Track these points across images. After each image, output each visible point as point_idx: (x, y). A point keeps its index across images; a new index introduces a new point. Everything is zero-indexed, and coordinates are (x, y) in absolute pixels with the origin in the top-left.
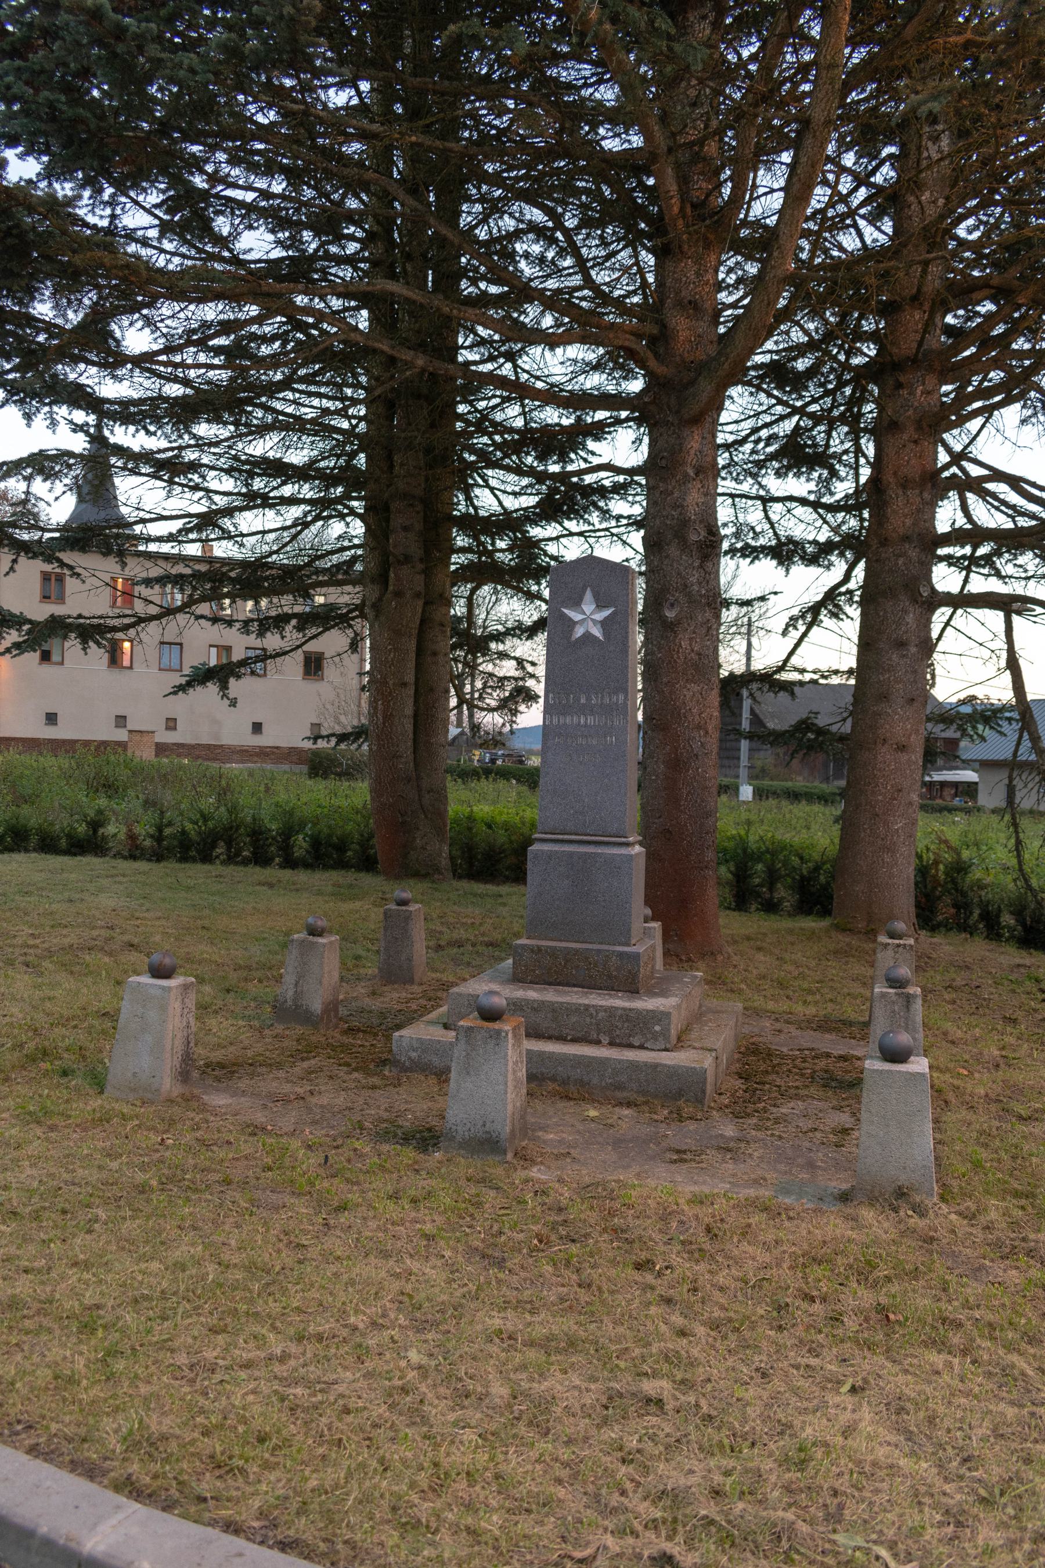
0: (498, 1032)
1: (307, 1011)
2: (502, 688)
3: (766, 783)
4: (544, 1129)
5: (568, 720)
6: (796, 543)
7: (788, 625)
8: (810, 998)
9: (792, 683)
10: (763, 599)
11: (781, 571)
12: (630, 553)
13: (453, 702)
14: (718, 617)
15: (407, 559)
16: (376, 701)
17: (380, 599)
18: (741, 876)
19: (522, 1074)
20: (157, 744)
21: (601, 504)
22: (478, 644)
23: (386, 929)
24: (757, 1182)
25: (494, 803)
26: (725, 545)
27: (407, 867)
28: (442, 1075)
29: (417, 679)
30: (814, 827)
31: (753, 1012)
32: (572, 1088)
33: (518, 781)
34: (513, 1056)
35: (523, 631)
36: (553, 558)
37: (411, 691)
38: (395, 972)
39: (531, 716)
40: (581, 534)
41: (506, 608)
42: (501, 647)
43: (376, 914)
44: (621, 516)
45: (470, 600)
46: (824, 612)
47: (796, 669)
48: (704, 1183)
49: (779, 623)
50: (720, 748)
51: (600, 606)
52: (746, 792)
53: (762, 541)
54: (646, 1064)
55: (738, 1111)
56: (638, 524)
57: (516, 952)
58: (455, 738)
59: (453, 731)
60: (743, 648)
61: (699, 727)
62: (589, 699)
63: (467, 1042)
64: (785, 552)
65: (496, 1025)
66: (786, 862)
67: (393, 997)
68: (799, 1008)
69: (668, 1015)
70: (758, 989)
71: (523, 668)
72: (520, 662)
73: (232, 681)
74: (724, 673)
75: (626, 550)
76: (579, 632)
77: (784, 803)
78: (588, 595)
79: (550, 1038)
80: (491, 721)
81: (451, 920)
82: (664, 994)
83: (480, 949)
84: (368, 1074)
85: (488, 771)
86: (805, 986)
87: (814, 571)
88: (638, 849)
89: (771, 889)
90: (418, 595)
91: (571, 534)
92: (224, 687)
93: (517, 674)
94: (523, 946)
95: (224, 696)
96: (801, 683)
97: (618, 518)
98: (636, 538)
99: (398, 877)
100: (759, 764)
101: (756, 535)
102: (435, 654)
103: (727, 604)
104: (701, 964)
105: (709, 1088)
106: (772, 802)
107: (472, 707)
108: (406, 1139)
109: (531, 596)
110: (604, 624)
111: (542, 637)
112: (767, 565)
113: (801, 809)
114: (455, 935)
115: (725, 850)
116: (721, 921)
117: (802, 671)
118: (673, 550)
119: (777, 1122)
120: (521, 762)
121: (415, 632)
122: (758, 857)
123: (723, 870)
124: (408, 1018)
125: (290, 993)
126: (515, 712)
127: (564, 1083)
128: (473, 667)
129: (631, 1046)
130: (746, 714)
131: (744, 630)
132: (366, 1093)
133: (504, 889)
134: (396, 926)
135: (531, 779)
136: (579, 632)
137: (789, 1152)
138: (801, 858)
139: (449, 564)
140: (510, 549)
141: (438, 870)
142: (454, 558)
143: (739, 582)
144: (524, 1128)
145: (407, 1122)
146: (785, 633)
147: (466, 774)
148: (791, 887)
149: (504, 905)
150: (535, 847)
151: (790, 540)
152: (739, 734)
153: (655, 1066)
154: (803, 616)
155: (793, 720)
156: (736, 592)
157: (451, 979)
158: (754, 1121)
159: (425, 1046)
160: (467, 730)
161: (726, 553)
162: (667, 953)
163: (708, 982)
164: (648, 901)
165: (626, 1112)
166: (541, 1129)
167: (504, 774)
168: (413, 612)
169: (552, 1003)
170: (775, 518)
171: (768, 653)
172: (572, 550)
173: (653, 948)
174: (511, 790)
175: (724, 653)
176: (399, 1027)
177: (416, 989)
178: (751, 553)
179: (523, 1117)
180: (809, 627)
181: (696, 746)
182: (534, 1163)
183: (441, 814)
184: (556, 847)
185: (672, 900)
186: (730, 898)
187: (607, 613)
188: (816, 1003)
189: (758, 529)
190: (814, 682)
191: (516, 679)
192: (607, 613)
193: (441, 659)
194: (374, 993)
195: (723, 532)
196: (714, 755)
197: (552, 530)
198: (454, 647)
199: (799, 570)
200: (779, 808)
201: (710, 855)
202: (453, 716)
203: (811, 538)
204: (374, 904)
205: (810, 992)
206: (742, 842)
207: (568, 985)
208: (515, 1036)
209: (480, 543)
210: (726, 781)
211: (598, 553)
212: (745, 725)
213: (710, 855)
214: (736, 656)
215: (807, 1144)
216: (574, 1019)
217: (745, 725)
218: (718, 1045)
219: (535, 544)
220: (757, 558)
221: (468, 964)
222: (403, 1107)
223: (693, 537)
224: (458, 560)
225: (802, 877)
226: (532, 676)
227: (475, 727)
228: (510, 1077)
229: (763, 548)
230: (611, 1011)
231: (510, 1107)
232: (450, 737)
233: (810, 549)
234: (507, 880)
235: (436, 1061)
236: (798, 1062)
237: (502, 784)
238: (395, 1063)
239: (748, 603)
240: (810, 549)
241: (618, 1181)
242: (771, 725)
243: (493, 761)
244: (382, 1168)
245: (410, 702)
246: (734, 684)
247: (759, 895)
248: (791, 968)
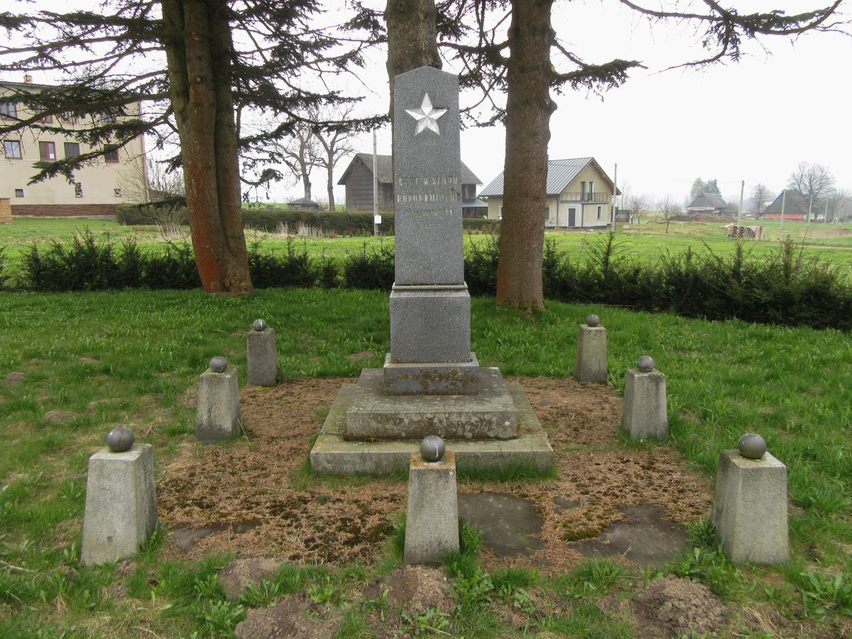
1: (221, 429)
20: (12, 206)
29: (217, 165)
37: (213, 172)
62: (430, 181)
73: (74, 172)
76: (420, 129)
78: (426, 100)
92: (69, 175)
95: (71, 182)
102: (227, 146)
110: (439, 121)
125: (205, 418)
136: (420, 129)
184: (411, 295)
187: (441, 113)
192: (441, 113)
245: (214, 179)
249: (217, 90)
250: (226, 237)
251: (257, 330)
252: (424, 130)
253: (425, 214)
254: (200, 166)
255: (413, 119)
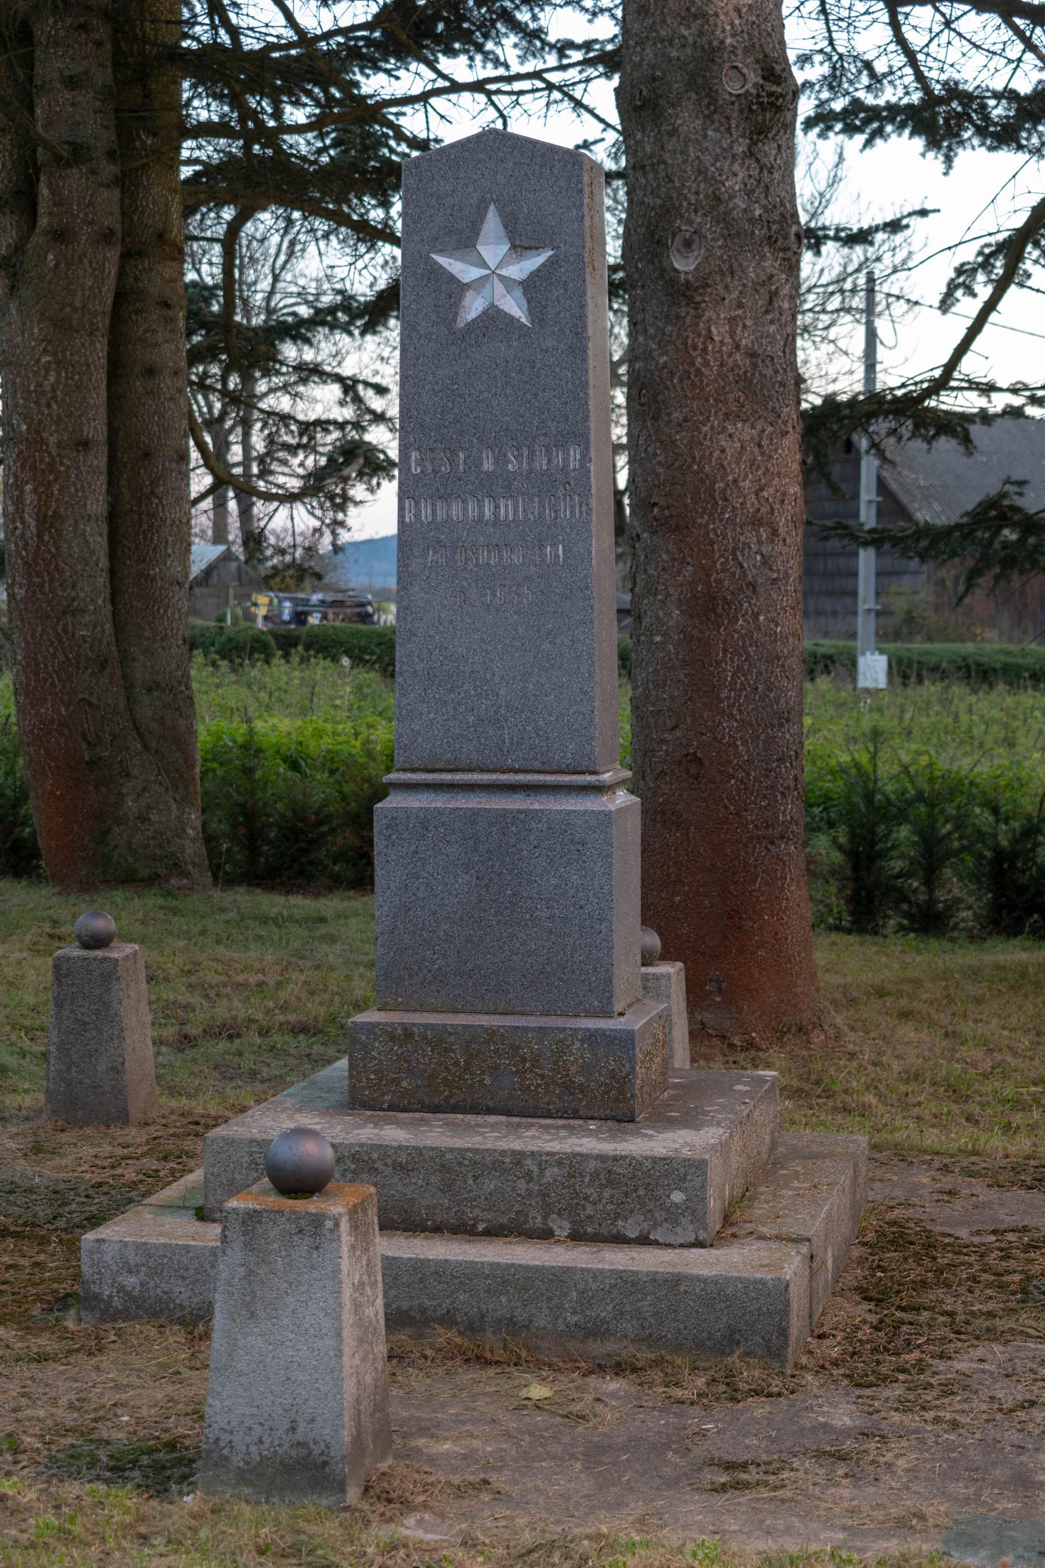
0: (317, 1221)
2: (310, 447)
3: (918, 646)
4: (428, 1430)
5: (456, 510)
6: (967, 98)
7: (952, 287)
8: (1018, 1119)
9: (965, 418)
10: (895, 226)
11: (934, 161)
12: (591, 129)
13: (201, 481)
14: (794, 268)
15: (78, 154)
16: (18, 485)
17: (19, 248)
18: (863, 857)
19: (376, 1309)
21: (523, 16)
22: (253, 348)
23: (59, 1003)
24: (902, 1525)
25: (304, 711)
26: (806, 106)
27: (106, 862)
28: (195, 1323)
30: (1024, 741)
31: (891, 1155)
32: (490, 1337)
33: (358, 660)
34: (352, 1271)
35: (354, 315)
36: (415, 143)
37: (99, 459)
38: (85, 1100)
39: (375, 513)
40: (478, 87)
41: (318, 263)
42: (309, 355)
43: (38, 972)
44: (570, 45)
45: (230, 241)
46: (1031, 252)
47: (973, 385)
48: (788, 1531)
49: (930, 280)
50: (808, 572)
51: (519, 247)
52: (873, 669)
53: (889, 95)
54: (654, 1278)
55: (862, 1368)
56: (608, 60)
57: (354, 1043)
58: (209, 571)
59: (203, 553)
60: (857, 344)
61: (756, 522)
62: (500, 460)
63: (248, 1246)
64: (942, 118)
65: (312, 1205)
66: (960, 823)
67: (81, 1156)
68: (995, 1142)
69: (700, 1166)
70: (904, 1103)
71: (358, 400)
72: (349, 386)
74: (812, 400)
75: (582, 121)
76: (473, 307)
77: (958, 690)
78: (492, 222)
79: (437, 1229)
80: (289, 523)
81: (213, 978)
82: (691, 1120)
83: (278, 1039)
84: (29, 1329)
85: (288, 641)
86: (1009, 1091)
87: (1008, 159)
88: (622, 798)
89: (929, 882)
90: (107, 236)
91: (456, 87)
93: (348, 413)
94: (371, 1027)
96: (984, 417)
97: (563, 47)
98: (602, 93)
99: (87, 887)
100: (900, 605)
101: (877, 80)
102: (151, 372)
103: (815, 239)
104: (776, 1054)
105: (796, 1325)
106: (931, 689)
107: (246, 493)
108: (118, 1469)
109: (370, 235)
110: (530, 286)
111: (393, 330)
112: (903, 147)
113: (992, 704)
114: (222, 1012)
115: (827, 799)
116: (820, 957)
117: (988, 389)
118: (687, 119)
119: (947, 1390)
120: (365, 618)
121: (103, 322)
122: (895, 812)
123: (822, 843)
124: (112, 1200)
126: (342, 503)
127: (473, 1327)
128: (242, 401)
129: (619, 1240)
130: (868, 492)
131: (858, 302)
132: (24, 1370)
133: (331, 904)
134: (83, 993)
135: (374, 652)
136: (473, 307)
137: (976, 1456)
138: (995, 810)
139: (176, 163)
140: (315, 125)
141: (177, 868)
142: (188, 149)
143: (843, 195)
144: (382, 1433)
145: (120, 1431)
146: (946, 304)
147: (240, 650)
148: (975, 877)
149: (332, 939)
150: (393, 802)
151: (953, 91)
152: (857, 538)
153: (674, 1282)
154: (986, 265)
155: (970, 501)
156: (841, 213)
157: (213, 1108)
158: (897, 1391)
159: (156, 1261)
160: (238, 549)
161: (809, 124)
162: (698, 1034)
163: (796, 1094)
164: (651, 915)
165: (613, 1385)
166: (423, 1431)
167: (325, 646)
168: (98, 274)
169: (441, 1152)
170: (916, 39)
171: (911, 352)
172: (458, 121)
173: (665, 1019)
174: (339, 681)
175: (810, 355)
176: (95, 1221)
177: (135, 1135)
178: (865, 121)
179: (380, 1407)
180: (1001, 287)
181: (751, 564)
182: (407, 1506)
183: (181, 740)
184: (439, 802)
185: (708, 914)
186: (838, 904)
187: (535, 261)
188: (1032, 1127)
189: (880, 67)
190: (1014, 413)
191: (341, 426)
192: (535, 261)
193: (166, 383)
194: (37, 1149)
195: (800, 76)
196: (792, 585)
197: (413, 78)
198: (196, 356)
199: (976, 159)
200: (946, 702)
201: (790, 809)
202: (202, 517)
203: (998, 85)
204: (34, 950)
205: (1018, 1104)
206: (864, 781)
207: (475, 1109)
208: (355, 1227)
209: (247, 114)
210: (827, 645)
211: (520, 126)
212: (867, 517)
213: (790, 809)
214: (841, 363)
215: (1015, 1437)
216: (490, 1185)
217: (867, 517)
218: (815, 1228)
219: (372, 112)
220: (879, 133)
221: (253, 1074)
222: (109, 1399)
223: (732, 87)
224: (195, 153)
225: (999, 854)
226: (379, 418)
227: (254, 539)
228: (348, 1318)
229: (893, 110)
230: (572, 1163)
231: (349, 1387)
232: (196, 569)
233: (998, 111)
234: (336, 884)
235: (182, 1293)
236: (992, 1258)
237: (320, 668)
238: (89, 1301)
239: (862, 237)
240: (998, 111)
241: (598, 1537)
242: (923, 516)
243: (300, 618)
244: (66, 1536)
245: (100, 484)
246: (838, 428)
247: (903, 897)
248: (978, 1054)
249: (127, 184)
250: (129, 686)
251: (86, 946)
252: (485, 313)
253: (483, 556)
254: (53, 440)
255: (452, 279)
